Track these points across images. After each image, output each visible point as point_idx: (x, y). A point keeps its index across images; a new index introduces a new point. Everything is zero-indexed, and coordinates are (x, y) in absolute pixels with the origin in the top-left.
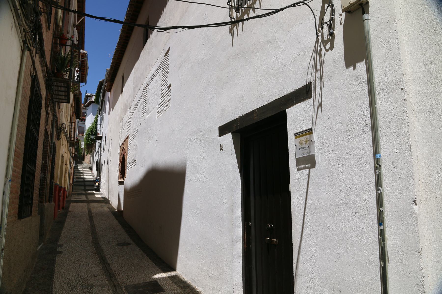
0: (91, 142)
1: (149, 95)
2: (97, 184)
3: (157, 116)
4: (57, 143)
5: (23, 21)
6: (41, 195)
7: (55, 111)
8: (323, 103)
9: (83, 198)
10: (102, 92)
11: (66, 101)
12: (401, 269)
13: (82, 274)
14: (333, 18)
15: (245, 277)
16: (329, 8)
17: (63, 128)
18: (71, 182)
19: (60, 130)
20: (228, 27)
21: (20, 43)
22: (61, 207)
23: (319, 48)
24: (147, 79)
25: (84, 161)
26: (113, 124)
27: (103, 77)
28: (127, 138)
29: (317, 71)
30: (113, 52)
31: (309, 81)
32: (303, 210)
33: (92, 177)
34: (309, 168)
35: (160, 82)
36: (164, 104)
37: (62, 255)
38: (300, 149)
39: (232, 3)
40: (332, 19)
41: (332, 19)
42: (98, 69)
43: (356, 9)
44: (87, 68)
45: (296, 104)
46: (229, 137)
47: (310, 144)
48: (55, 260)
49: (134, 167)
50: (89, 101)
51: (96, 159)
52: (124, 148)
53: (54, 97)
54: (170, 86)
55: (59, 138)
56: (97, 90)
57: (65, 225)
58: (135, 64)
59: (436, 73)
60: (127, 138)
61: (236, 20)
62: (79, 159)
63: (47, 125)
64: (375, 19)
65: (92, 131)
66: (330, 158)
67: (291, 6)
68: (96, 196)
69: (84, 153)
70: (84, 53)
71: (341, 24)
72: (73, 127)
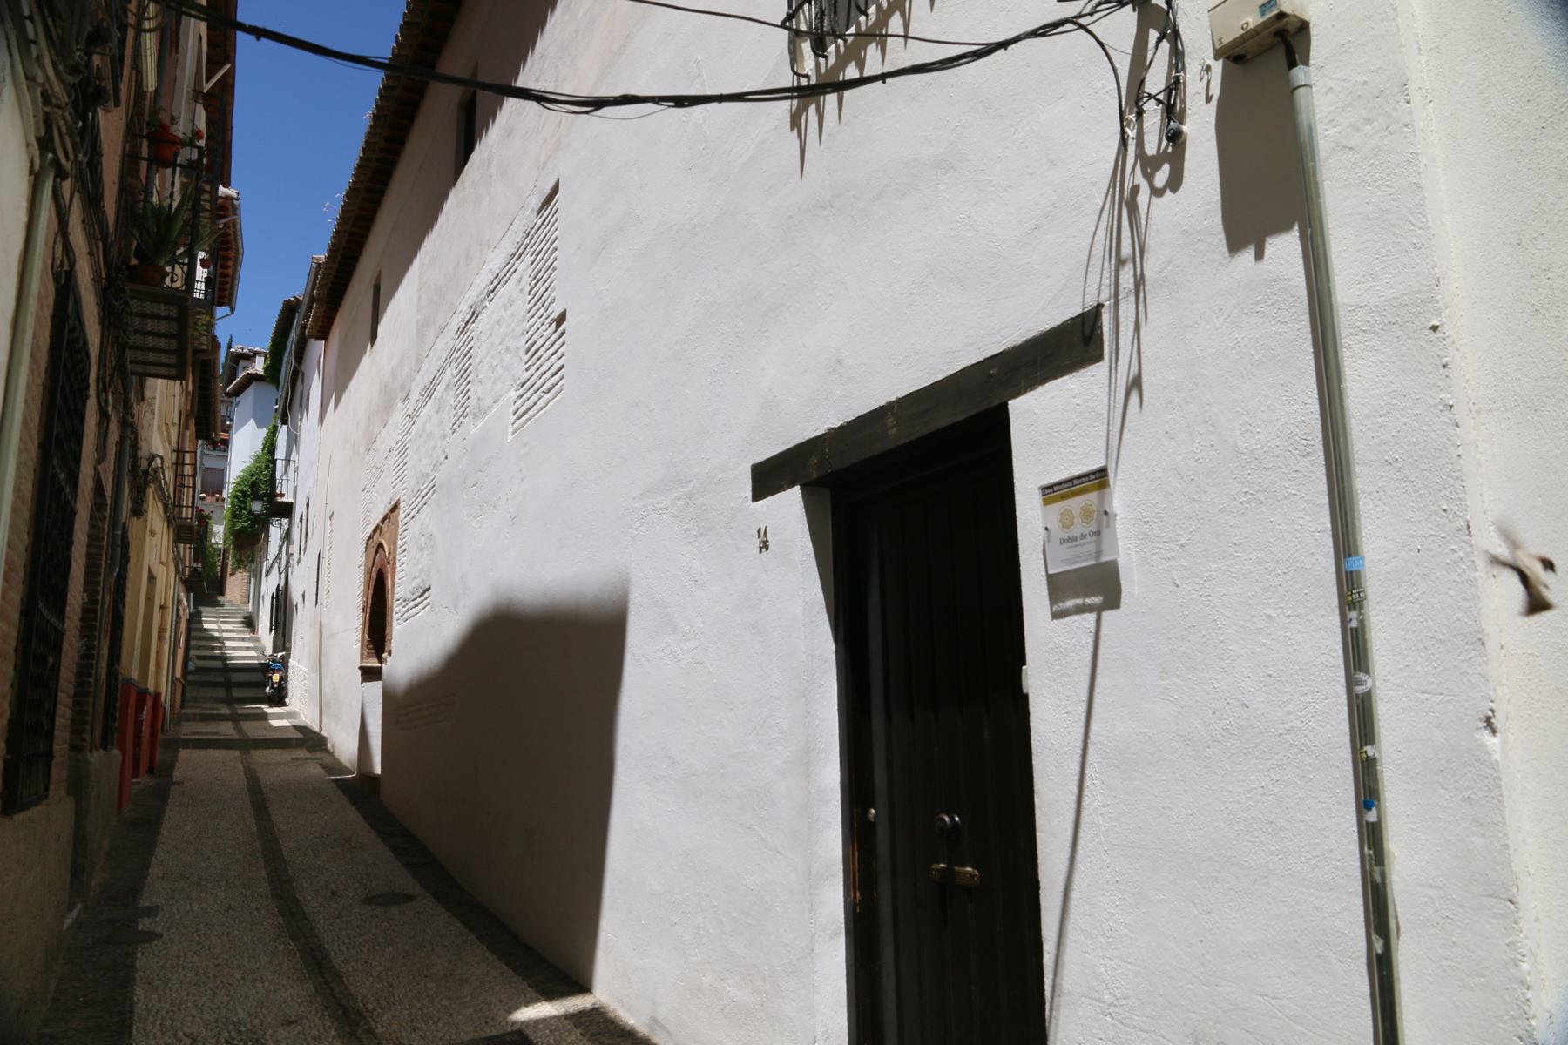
0: (252, 525)
1: (479, 352)
2: (276, 678)
3: (511, 429)
4: (134, 525)
5: (47, 62)
6: (77, 726)
7: (127, 407)
8: (1144, 379)
9: (226, 730)
10: (293, 339)
11: (173, 372)
12: (1445, 963)
13: (242, 1015)
14: (1177, 78)
15: (857, 1007)
16: (1165, 45)
17: (156, 470)
18: (178, 674)
19: (139, 476)
20: (784, 107)
21: (28, 145)
22: (144, 764)
23: (1128, 185)
24: (473, 295)
25: (222, 593)
26: (339, 459)
27: (297, 286)
28: (395, 508)
29: (1121, 262)
30: (340, 196)
31: (1090, 303)
32: (1078, 758)
33: (253, 653)
34: (1098, 610)
35: (522, 304)
36: (540, 387)
37: (157, 944)
38: (1063, 541)
39: (798, 23)
40: (1175, 85)
41: (1175, 85)
42: (279, 253)
43: (1267, 50)
44: (237, 253)
45: (1043, 381)
46: (791, 501)
47: (1100, 525)
48: (133, 966)
49: (423, 614)
50: (241, 375)
51: (269, 585)
52: (380, 546)
53: (129, 354)
54: (561, 319)
55: (138, 511)
56: (276, 333)
57: (164, 831)
58: (423, 239)
59: (1550, 275)
60: (395, 508)
61: (813, 81)
62: (205, 586)
63: (101, 459)
64: (1331, 83)
65: (253, 485)
66: (1175, 574)
67: (1034, 34)
68: (275, 723)
69: (224, 566)
70: (228, 198)
71: (1209, 99)
72: (188, 470)
